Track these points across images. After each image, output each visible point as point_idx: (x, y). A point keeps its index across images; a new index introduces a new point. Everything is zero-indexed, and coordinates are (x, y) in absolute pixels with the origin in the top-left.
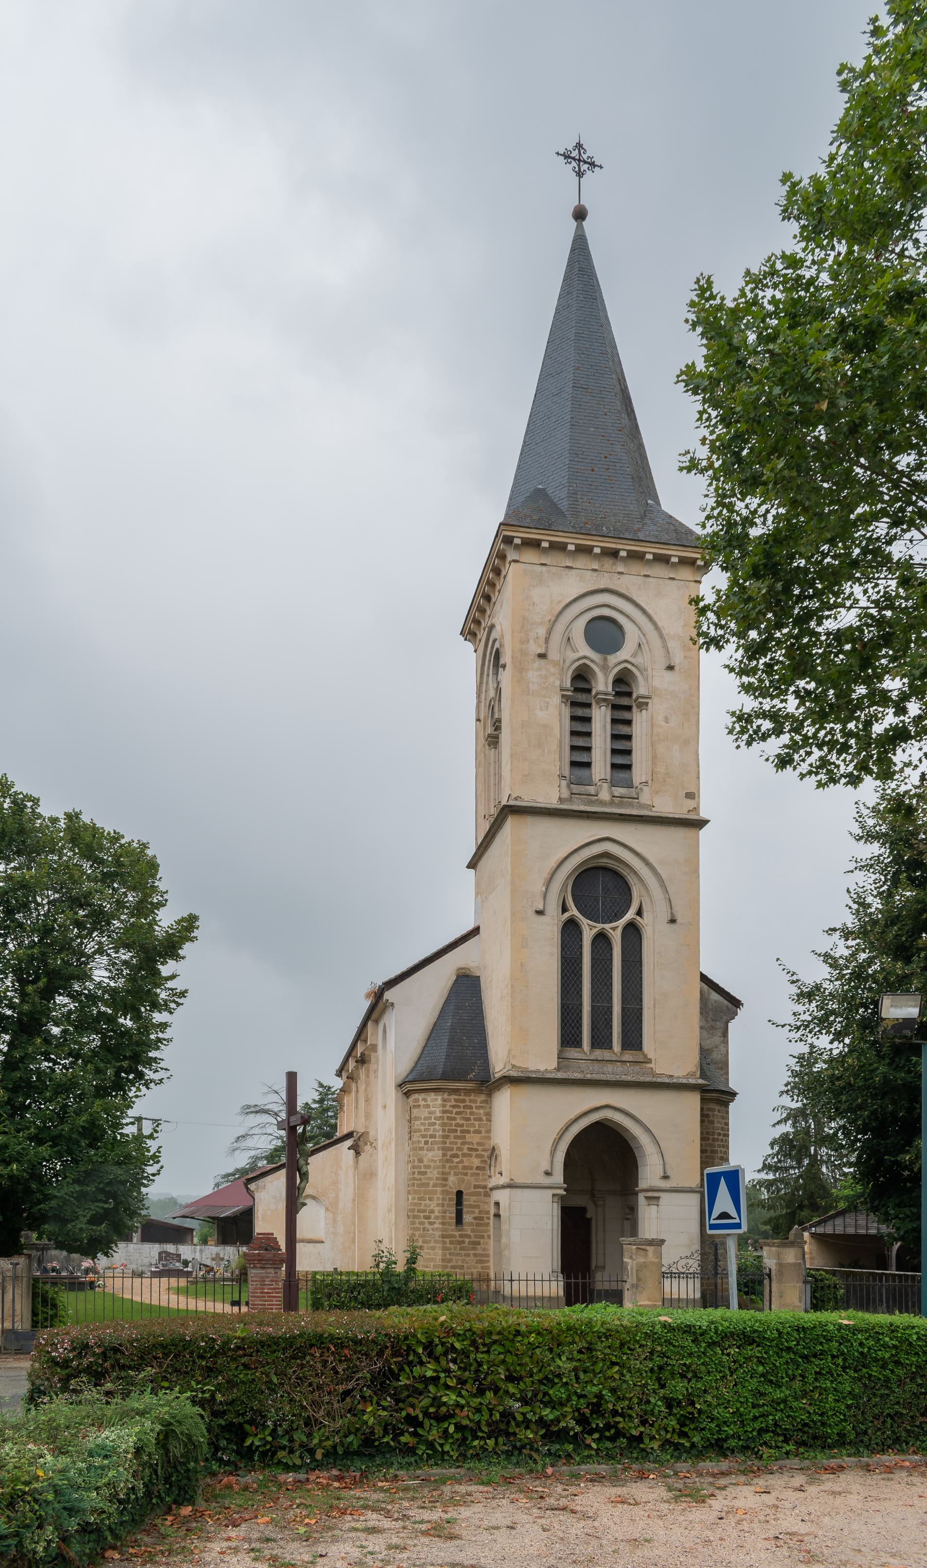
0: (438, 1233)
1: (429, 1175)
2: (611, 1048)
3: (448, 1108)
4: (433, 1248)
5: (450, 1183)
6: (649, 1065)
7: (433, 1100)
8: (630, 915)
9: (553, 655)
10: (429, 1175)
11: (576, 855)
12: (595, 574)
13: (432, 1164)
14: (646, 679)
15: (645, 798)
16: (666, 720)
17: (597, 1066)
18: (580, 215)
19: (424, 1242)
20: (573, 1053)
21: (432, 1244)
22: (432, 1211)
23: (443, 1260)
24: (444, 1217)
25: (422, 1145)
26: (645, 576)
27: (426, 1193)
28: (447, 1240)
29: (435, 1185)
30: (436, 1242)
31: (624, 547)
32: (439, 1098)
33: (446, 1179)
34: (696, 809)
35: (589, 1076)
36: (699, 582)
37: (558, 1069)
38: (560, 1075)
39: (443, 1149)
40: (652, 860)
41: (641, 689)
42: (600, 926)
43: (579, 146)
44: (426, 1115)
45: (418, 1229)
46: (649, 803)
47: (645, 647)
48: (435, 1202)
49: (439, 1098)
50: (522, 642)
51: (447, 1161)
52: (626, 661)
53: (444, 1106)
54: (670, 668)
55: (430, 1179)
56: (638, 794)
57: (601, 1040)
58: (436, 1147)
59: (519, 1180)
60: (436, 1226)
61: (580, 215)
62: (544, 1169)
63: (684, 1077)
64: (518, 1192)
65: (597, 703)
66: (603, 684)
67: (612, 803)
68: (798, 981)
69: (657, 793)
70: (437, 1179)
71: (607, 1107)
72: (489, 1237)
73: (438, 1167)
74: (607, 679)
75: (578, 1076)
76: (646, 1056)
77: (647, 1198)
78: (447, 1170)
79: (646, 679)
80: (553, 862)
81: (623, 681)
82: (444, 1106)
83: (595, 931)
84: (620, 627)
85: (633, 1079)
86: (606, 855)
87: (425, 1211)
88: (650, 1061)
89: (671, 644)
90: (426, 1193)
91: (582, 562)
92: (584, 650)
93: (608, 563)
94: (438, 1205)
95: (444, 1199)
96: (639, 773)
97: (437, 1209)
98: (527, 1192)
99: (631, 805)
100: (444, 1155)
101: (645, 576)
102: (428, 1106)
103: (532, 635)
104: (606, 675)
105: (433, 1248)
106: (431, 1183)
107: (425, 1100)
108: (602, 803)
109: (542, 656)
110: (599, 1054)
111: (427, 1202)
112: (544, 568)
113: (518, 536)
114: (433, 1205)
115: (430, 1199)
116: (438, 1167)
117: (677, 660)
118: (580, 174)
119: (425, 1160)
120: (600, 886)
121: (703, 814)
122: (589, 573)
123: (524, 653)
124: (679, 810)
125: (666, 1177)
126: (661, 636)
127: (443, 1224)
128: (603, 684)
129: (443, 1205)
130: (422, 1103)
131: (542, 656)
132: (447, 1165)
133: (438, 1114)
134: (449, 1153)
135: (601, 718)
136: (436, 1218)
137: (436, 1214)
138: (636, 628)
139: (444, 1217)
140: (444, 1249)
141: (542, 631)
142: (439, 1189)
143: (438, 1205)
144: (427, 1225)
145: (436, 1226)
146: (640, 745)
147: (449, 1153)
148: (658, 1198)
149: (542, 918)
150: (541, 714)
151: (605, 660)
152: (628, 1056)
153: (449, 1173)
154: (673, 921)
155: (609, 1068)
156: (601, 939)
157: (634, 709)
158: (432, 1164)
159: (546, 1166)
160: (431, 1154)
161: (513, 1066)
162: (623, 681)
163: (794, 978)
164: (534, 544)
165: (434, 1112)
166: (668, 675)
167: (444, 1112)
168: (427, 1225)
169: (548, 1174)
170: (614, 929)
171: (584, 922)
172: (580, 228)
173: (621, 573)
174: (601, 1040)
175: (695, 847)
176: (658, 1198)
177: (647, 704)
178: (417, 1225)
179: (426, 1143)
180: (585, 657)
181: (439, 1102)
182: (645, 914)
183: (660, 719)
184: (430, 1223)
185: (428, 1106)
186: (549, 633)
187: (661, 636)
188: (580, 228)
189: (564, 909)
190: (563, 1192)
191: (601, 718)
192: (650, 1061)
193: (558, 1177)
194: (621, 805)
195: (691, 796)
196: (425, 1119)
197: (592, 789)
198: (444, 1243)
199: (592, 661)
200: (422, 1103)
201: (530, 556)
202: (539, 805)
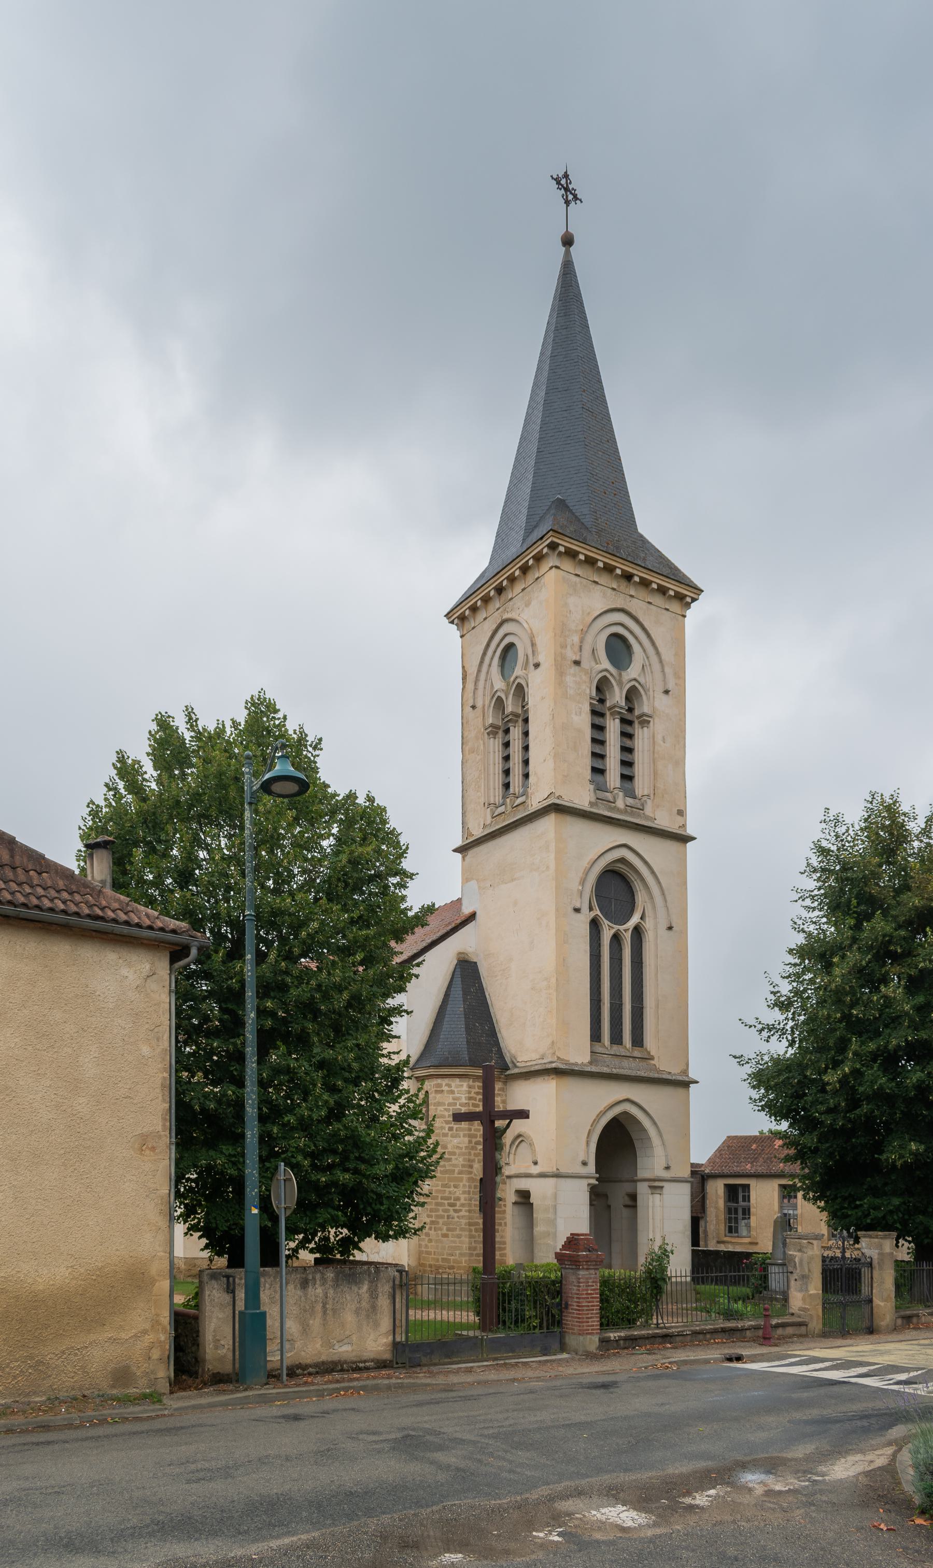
0: (464, 1221)
1: (454, 1162)
2: (621, 1044)
3: (472, 1095)
4: (459, 1236)
5: (475, 1171)
6: (652, 1062)
7: (457, 1086)
8: (635, 920)
9: (584, 664)
10: (454, 1162)
11: (602, 858)
12: (614, 593)
13: (457, 1151)
14: (648, 699)
15: (648, 811)
16: (664, 740)
17: (616, 1061)
18: (568, 241)
19: (448, 1230)
20: (599, 1049)
21: (458, 1232)
22: (458, 1199)
23: (470, 1248)
24: (470, 1205)
25: (446, 1131)
26: (649, 603)
27: (450, 1179)
28: (473, 1228)
29: (460, 1173)
30: (462, 1229)
31: (638, 574)
32: (465, 1084)
33: (471, 1167)
34: (684, 826)
35: (615, 1071)
36: (684, 616)
37: (591, 1063)
38: (593, 1069)
39: (470, 1136)
40: (655, 870)
41: (644, 707)
42: (617, 927)
43: (566, 176)
44: (451, 1101)
45: (442, 1217)
46: (651, 815)
47: (647, 669)
48: (461, 1189)
49: (465, 1084)
50: (562, 647)
51: (473, 1148)
52: (635, 680)
53: (470, 1092)
54: (667, 692)
55: (455, 1166)
56: (643, 805)
57: (617, 1038)
58: (461, 1133)
59: (563, 1170)
60: (461, 1214)
61: (568, 241)
62: (581, 1159)
63: (679, 1074)
64: (560, 1180)
65: (611, 714)
66: (617, 697)
67: (625, 812)
68: (778, 992)
69: (658, 806)
70: (463, 1166)
71: (628, 1100)
72: (505, 1224)
73: (464, 1154)
74: (621, 693)
75: (605, 1070)
76: (649, 1053)
77: (650, 1187)
78: (472, 1157)
79: (648, 699)
80: (585, 863)
81: (632, 695)
82: (470, 1092)
83: (613, 931)
84: (628, 647)
85: (646, 1075)
86: (623, 860)
87: (449, 1198)
88: (652, 1058)
89: (667, 670)
90: (450, 1179)
91: (604, 579)
92: (606, 664)
93: (624, 584)
94: (464, 1192)
95: (470, 1187)
96: (641, 785)
97: (462, 1197)
98: (569, 1181)
99: (639, 816)
100: (470, 1142)
101: (649, 603)
102: (452, 1092)
103: (569, 641)
104: (621, 689)
105: (459, 1236)
106: (457, 1170)
107: (449, 1086)
108: (618, 810)
109: (577, 663)
110: (616, 1049)
111: (452, 1189)
112: (578, 579)
113: (564, 544)
114: (458, 1192)
115: (455, 1187)
116: (464, 1154)
117: (670, 686)
118: (567, 203)
119: (449, 1146)
120: (616, 888)
121: (690, 831)
122: (610, 590)
123: (563, 657)
124: (673, 827)
125: (668, 1168)
126: (661, 661)
127: (469, 1211)
128: (617, 697)
129: (469, 1193)
130: (445, 1088)
131: (577, 663)
132: (473, 1152)
133: (464, 1101)
134: (474, 1140)
135: (613, 728)
136: (462, 1205)
137: (462, 1201)
138: (641, 650)
139: (470, 1205)
140: (471, 1237)
141: (576, 639)
142: (465, 1176)
143: (464, 1192)
144: (452, 1213)
145: (461, 1214)
146: (641, 758)
147: (474, 1140)
148: (662, 1187)
149: (578, 915)
150: (576, 719)
151: (620, 675)
152: (637, 1053)
153: (473, 1161)
154: (670, 928)
155: (625, 1063)
156: (616, 938)
157: (636, 725)
158: (457, 1151)
159: (582, 1157)
160: (455, 1141)
161: (558, 1058)
162: (632, 695)
163: (776, 989)
164: (571, 554)
165: (458, 1099)
166: (664, 697)
167: (470, 1098)
168: (452, 1213)
169: (584, 1164)
170: (625, 931)
171: (605, 923)
172: (567, 254)
173: (632, 596)
174: (617, 1038)
175: (682, 861)
176: (662, 1187)
177: (649, 722)
178: (441, 1213)
179: (451, 1129)
180: (606, 670)
181: (465, 1088)
182: (647, 919)
183: (659, 738)
184: (455, 1211)
185: (452, 1092)
186: (582, 641)
187: (661, 661)
188: (567, 254)
189: (591, 909)
190: (594, 1182)
191: (613, 728)
192: (652, 1058)
193: (591, 1168)
194: (632, 814)
195: (681, 813)
196: (449, 1104)
197: (609, 796)
198: (470, 1231)
199: (612, 675)
200: (445, 1088)
201: (567, 565)
202: (575, 806)
